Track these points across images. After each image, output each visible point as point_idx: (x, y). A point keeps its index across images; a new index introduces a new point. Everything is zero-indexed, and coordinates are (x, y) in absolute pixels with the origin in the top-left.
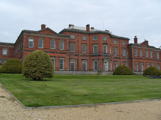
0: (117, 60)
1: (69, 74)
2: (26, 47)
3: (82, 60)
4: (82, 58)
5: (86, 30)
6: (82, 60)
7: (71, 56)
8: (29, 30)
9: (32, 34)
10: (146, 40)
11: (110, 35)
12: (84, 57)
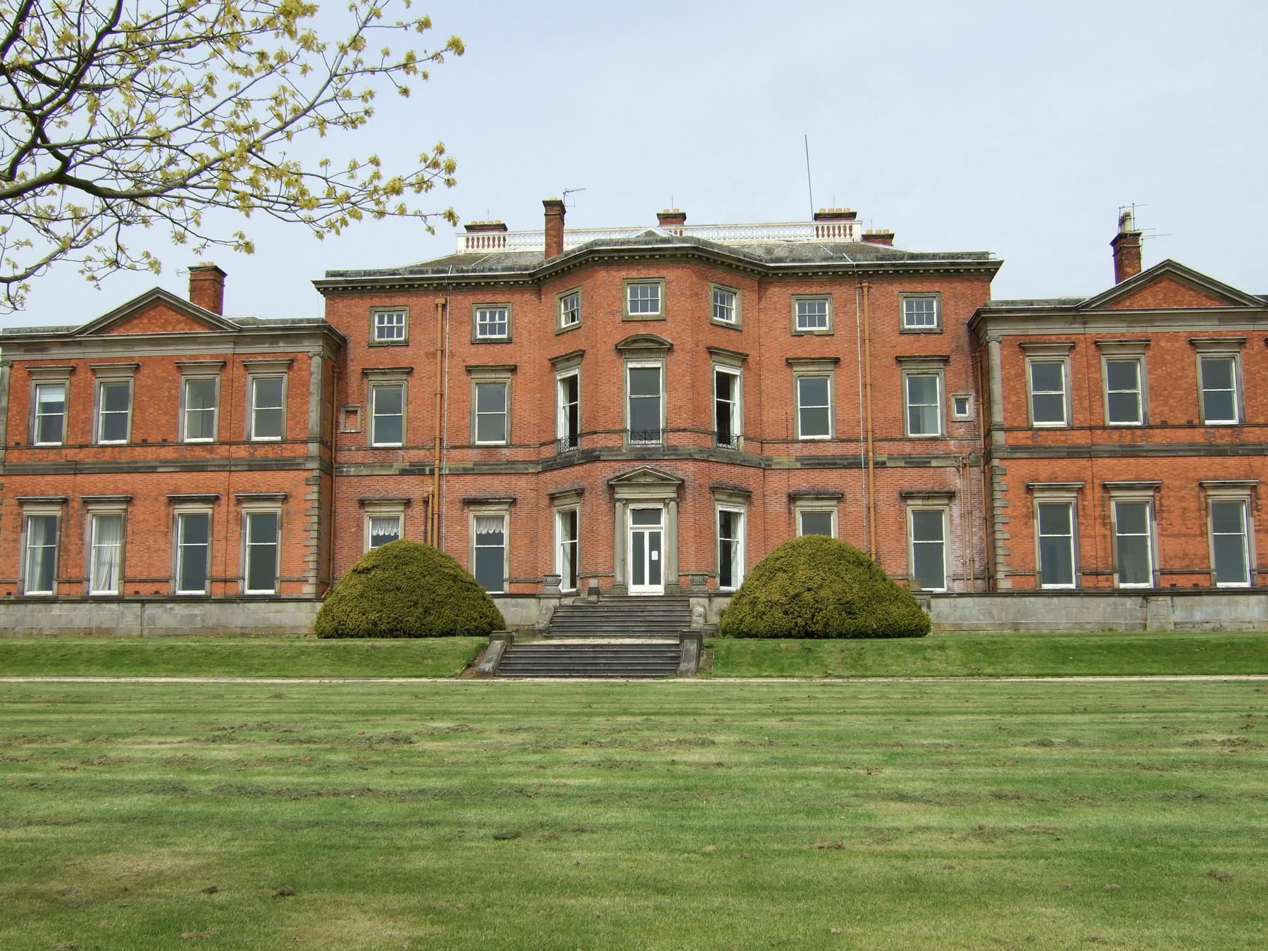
0: (831, 479)
1: (88, 633)
2: (18, 444)
3: (469, 502)
4: (473, 486)
5: (543, 248)
6: (469, 502)
7: (367, 481)
8: (37, 330)
9: (57, 353)
10: (1150, 259)
11: (704, 259)
12: (488, 480)
